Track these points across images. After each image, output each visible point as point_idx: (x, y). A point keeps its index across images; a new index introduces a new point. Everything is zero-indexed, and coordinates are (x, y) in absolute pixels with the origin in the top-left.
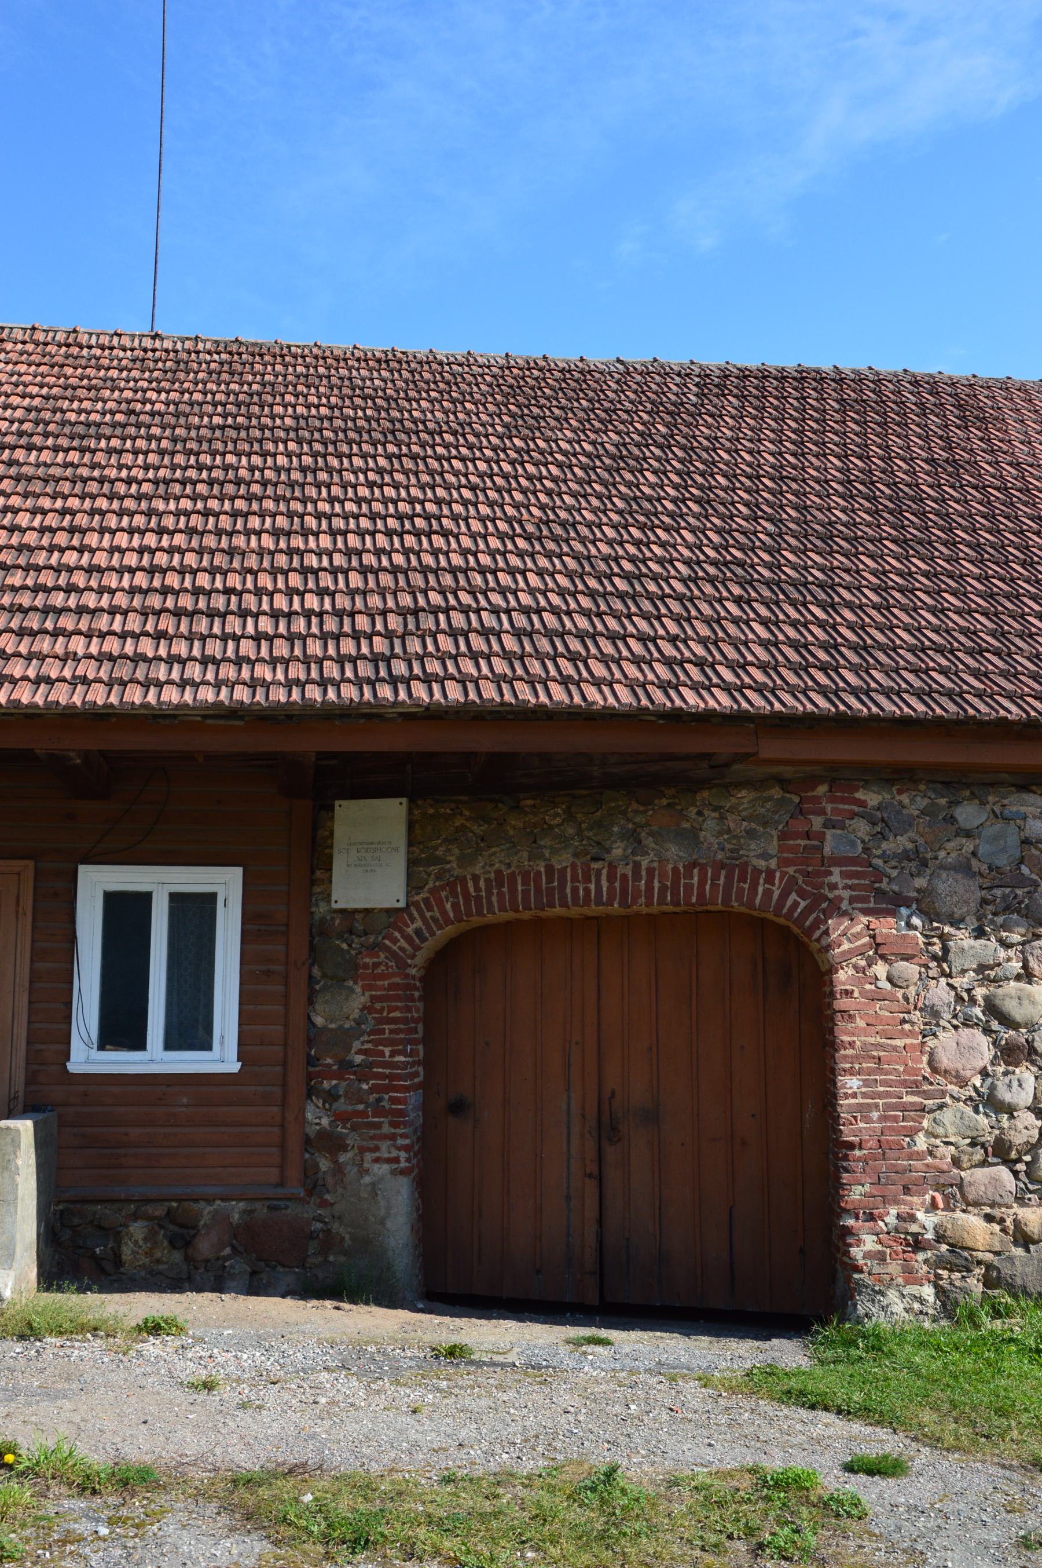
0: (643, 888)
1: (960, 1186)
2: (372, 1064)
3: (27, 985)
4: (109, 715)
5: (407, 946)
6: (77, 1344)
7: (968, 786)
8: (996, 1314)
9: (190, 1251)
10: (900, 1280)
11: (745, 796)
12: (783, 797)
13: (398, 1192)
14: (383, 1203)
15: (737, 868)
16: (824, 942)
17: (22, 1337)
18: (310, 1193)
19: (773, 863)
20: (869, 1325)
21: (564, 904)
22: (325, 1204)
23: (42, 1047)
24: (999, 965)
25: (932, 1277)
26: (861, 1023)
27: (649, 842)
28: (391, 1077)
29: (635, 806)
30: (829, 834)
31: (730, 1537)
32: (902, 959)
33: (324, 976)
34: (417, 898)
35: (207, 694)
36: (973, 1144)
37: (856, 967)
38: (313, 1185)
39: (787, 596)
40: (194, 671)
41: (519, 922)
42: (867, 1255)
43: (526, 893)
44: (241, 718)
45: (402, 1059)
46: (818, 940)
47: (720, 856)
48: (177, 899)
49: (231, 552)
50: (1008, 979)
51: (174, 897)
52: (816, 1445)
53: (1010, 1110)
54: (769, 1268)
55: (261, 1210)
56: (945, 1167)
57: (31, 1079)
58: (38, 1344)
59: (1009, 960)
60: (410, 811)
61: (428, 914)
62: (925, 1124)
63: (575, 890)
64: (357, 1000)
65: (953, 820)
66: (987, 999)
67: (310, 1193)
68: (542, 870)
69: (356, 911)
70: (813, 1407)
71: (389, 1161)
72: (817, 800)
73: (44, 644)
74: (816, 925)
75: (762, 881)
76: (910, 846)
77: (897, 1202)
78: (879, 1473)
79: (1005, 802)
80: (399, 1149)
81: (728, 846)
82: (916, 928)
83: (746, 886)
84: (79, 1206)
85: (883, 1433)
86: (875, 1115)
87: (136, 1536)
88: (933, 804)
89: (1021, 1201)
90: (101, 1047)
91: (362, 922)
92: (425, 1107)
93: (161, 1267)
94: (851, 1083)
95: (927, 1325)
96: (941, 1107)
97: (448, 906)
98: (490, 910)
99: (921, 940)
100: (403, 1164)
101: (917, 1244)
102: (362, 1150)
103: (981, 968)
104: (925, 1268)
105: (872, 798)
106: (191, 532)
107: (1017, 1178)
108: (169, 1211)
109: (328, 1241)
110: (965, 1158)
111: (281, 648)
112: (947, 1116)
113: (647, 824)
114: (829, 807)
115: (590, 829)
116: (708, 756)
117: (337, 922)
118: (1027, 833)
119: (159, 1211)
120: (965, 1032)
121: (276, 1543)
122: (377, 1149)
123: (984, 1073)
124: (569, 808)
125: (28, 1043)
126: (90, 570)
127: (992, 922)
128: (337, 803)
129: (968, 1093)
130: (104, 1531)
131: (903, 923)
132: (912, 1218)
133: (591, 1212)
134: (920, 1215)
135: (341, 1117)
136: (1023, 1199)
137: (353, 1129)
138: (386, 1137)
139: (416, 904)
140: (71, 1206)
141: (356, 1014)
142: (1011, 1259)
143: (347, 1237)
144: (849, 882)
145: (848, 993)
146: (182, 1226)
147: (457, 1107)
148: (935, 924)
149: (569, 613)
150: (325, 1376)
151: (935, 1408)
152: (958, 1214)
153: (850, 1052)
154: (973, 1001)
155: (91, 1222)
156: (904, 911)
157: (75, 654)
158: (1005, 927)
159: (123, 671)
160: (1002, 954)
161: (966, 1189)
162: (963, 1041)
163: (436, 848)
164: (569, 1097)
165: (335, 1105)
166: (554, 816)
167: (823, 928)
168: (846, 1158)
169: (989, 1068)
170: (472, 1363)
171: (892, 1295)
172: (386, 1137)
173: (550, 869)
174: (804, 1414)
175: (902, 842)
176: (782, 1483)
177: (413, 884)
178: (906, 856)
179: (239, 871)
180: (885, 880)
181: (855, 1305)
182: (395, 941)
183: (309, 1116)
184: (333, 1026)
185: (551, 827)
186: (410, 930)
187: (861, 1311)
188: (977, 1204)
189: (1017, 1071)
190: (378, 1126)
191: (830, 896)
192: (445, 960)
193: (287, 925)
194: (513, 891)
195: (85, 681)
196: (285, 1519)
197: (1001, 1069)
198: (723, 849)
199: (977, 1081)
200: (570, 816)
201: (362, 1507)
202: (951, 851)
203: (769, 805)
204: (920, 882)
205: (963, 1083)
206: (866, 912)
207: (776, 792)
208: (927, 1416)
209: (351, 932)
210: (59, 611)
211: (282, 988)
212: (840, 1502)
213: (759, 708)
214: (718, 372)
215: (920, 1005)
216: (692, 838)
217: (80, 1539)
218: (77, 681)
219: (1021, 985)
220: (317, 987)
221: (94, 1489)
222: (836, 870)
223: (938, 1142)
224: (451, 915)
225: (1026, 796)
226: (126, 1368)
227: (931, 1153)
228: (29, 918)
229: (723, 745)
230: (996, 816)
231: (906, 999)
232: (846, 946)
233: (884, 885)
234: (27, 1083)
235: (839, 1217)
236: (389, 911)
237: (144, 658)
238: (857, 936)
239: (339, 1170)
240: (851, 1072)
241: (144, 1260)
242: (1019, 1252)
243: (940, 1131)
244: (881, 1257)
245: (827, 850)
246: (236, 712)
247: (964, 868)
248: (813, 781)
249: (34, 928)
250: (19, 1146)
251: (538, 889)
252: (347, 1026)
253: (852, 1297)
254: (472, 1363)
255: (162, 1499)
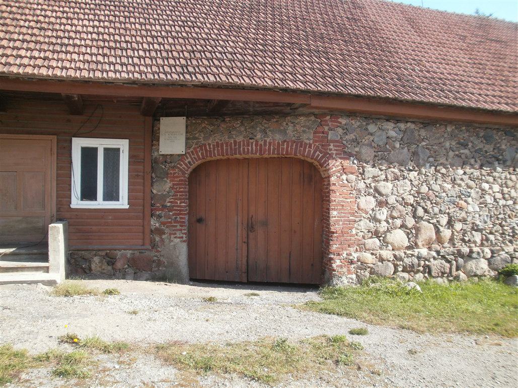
0: (267, 149)
1: (364, 245)
2: (173, 206)
3: (56, 178)
4: (89, 81)
5: (185, 167)
6: (85, 298)
7: (372, 119)
8: (373, 282)
9: (114, 266)
10: (346, 273)
11: (302, 119)
12: (315, 120)
13: (183, 248)
14: (178, 251)
15: (299, 143)
16: (327, 168)
17: (66, 296)
18: (153, 248)
19: (311, 142)
20: (337, 287)
21: (240, 154)
22: (158, 251)
23: (62, 199)
24: (379, 176)
25: (355, 272)
26: (338, 194)
27: (269, 133)
28: (180, 210)
29: (265, 121)
30: (330, 132)
31: (326, 359)
32: (351, 174)
33: (156, 176)
34: (189, 151)
35: (124, 75)
36: (368, 232)
37: (337, 176)
38: (154, 246)
39: (314, 54)
40: (118, 67)
41: (221, 159)
42: (337, 266)
43: (227, 150)
44: (137, 84)
45: (184, 204)
46: (325, 167)
47: (293, 139)
48: (106, 150)
49: (126, 29)
50: (381, 181)
51: (106, 150)
52: (337, 326)
53: (379, 221)
54: (306, 271)
55: (137, 253)
56: (360, 239)
57: (58, 210)
58: (72, 298)
59: (382, 175)
60: (187, 122)
61: (193, 156)
62: (355, 226)
63: (244, 149)
64: (167, 185)
66: (375, 187)
67: (153, 248)
68: (233, 142)
69: (167, 155)
70: (330, 314)
71: (179, 238)
72: (326, 121)
73: (63, 56)
74: (325, 161)
75: (307, 147)
76: (354, 137)
77: (346, 250)
78: (361, 334)
79: (383, 124)
80: (183, 234)
81: (296, 135)
82: (355, 164)
83: (302, 149)
84: (76, 252)
85: (354, 321)
86: (341, 223)
87: (129, 368)
88: (362, 124)
89: (380, 248)
90: (82, 200)
91: (169, 159)
92: (189, 220)
93: (105, 271)
94: (334, 213)
95: (354, 286)
96: (360, 221)
97: (200, 154)
98: (215, 156)
99: (357, 168)
100: (184, 239)
101: (352, 262)
102: (170, 234)
103: (374, 177)
104: (354, 269)
105: (343, 121)
106: (111, 22)
107: (380, 242)
108: (106, 254)
109: (159, 263)
110: (366, 236)
111: (148, 61)
112: (362, 223)
113: (269, 127)
114: (330, 124)
115: (249, 128)
116: (289, 105)
117: (161, 159)
118: (389, 135)
119: (103, 253)
120: (368, 197)
121: (179, 370)
122: (175, 234)
123: (373, 210)
124: (242, 121)
125: (57, 198)
126: (76, 32)
127: (377, 163)
128: (161, 118)
129: (368, 216)
130: (117, 367)
131: (351, 162)
132: (351, 255)
133: (245, 254)
134: (353, 254)
135: (163, 223)
136: (381, 248)
137: (167, 227)
138: (178, 230)
139: (188, 153)
140: (74, 252)
141: (168, 189)
142: (378, 266)
143: (166, 262)
144: (336, 148)
145: (334, 184)
146: (111, 258)
147: (200, 220)
148: (361, 163)
149: (245, 55)
150: (171, 308)
151: (365, 312)
152: (364, 253)
153: (334, 203)
154: (371, 187)
155: (81, 257)
156: (352, 158)
157: (75, 59)
158: (381, 164)
159: (94, 66)
160: (380, 173)
161: (366, 245)
162: (368, 200)
163: (196, 134)
164: (238, 217)
165: (161, 219)
166: (237, 124)
167: (327, 163)
168: (332, 236)
169: (375, 209)
170: (217, 303)
171: (344, 278)
172: (178, 230)
173: (235, 142)
174: (328, 316)
175: (351, 136)
176: (335, 340)
177: (188, 146)
178: (353, 141)
179: (127, 141)
180: (347, 148)
181: (333, 281)
182: (181, 165)
183: (152, 223)
184: (160, 193)
185: (236, 128)
186: (186, 162)
187: (334, 283)
188: (369, 250)
189: (382, 209)
190: (176, 226)
191: (330, 153)
192: (196, 171)
193: (144, 160)
194: (222, 149)
195: (80, 69)
196: (180, 361)
197: (377, 209)
198: (295, 137)
199: (371, 212)
200: (242, 124)
201: (205, 356)
202: (367, 139)
203: (310, 122)
204: (357, 149)
205: (367, 213)
206: (341, 158)
207: (313, 118)
208: (365, 315)
209: (166, 162)
210: (67, 45)
211: (142, 181)
212: (356, 345)
213: (313, 88)
215: (355, 188)
216: (284, 132)
217: (109, 370)
218: (76, 69)
219: (385, 182)
220: (154, 180)
221: (109, 351)
222: (332, 144)
223: (359, 231)
224: (201, 157)
225: (389, 123)
226: (105, 307)
227: (357, 235)
228: (56, 156)
229: (297, 101)
230: (380, 129)
231: (352, 187)
232: (334, 169)
233: (346, 150)
234: (57, 211)
235: (328, 254)
236: (179, 155)
237: (100, 63)
238: (338, 166)
239: (162, 240)
240: (334, 209)
241: (99, 269)
242: (380, 263)
243: (360, 228)
244: (341, 267)
245: (329, 138)
246: (134, 82)
247: (370, 145)
248: (325, 115)
249: (57, 159)
250: (59, 232)
251: (231, 149)
252: (164, 193)
253: (332, 279)
254: (217, 303)
255: (133, 355)
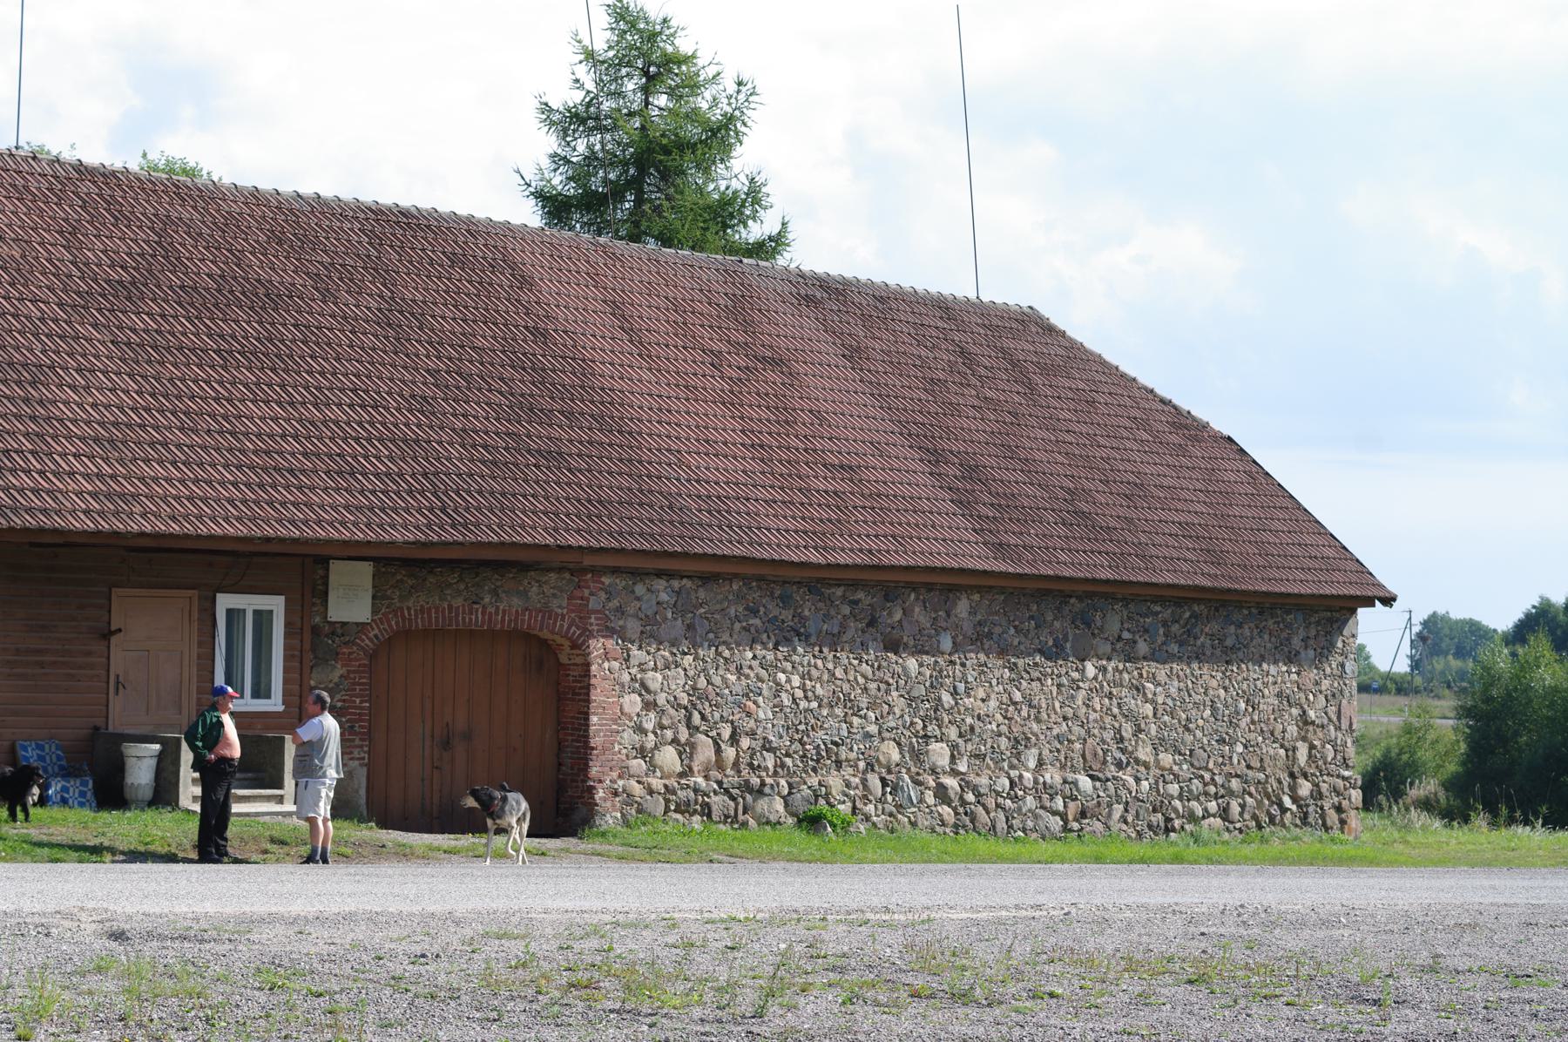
65: (633, 592)
94: (594, 719)
101: (616, 794)
105: (607, 580)
112: (625, 735)
141: (336, 680)
173: (450, 607)
177: (374, 612)
200: (461, 579)
204: (621, 623)
207: (567, 575)
214: (1446, 631)
216: (524, 594)
